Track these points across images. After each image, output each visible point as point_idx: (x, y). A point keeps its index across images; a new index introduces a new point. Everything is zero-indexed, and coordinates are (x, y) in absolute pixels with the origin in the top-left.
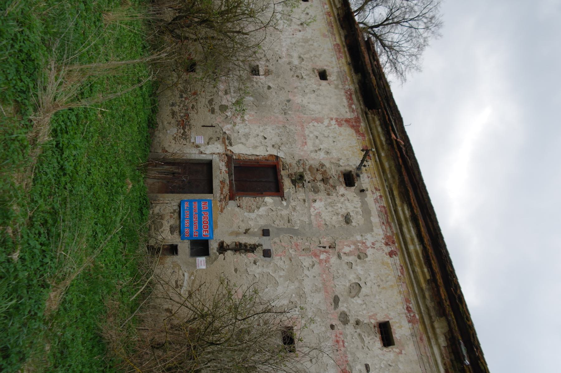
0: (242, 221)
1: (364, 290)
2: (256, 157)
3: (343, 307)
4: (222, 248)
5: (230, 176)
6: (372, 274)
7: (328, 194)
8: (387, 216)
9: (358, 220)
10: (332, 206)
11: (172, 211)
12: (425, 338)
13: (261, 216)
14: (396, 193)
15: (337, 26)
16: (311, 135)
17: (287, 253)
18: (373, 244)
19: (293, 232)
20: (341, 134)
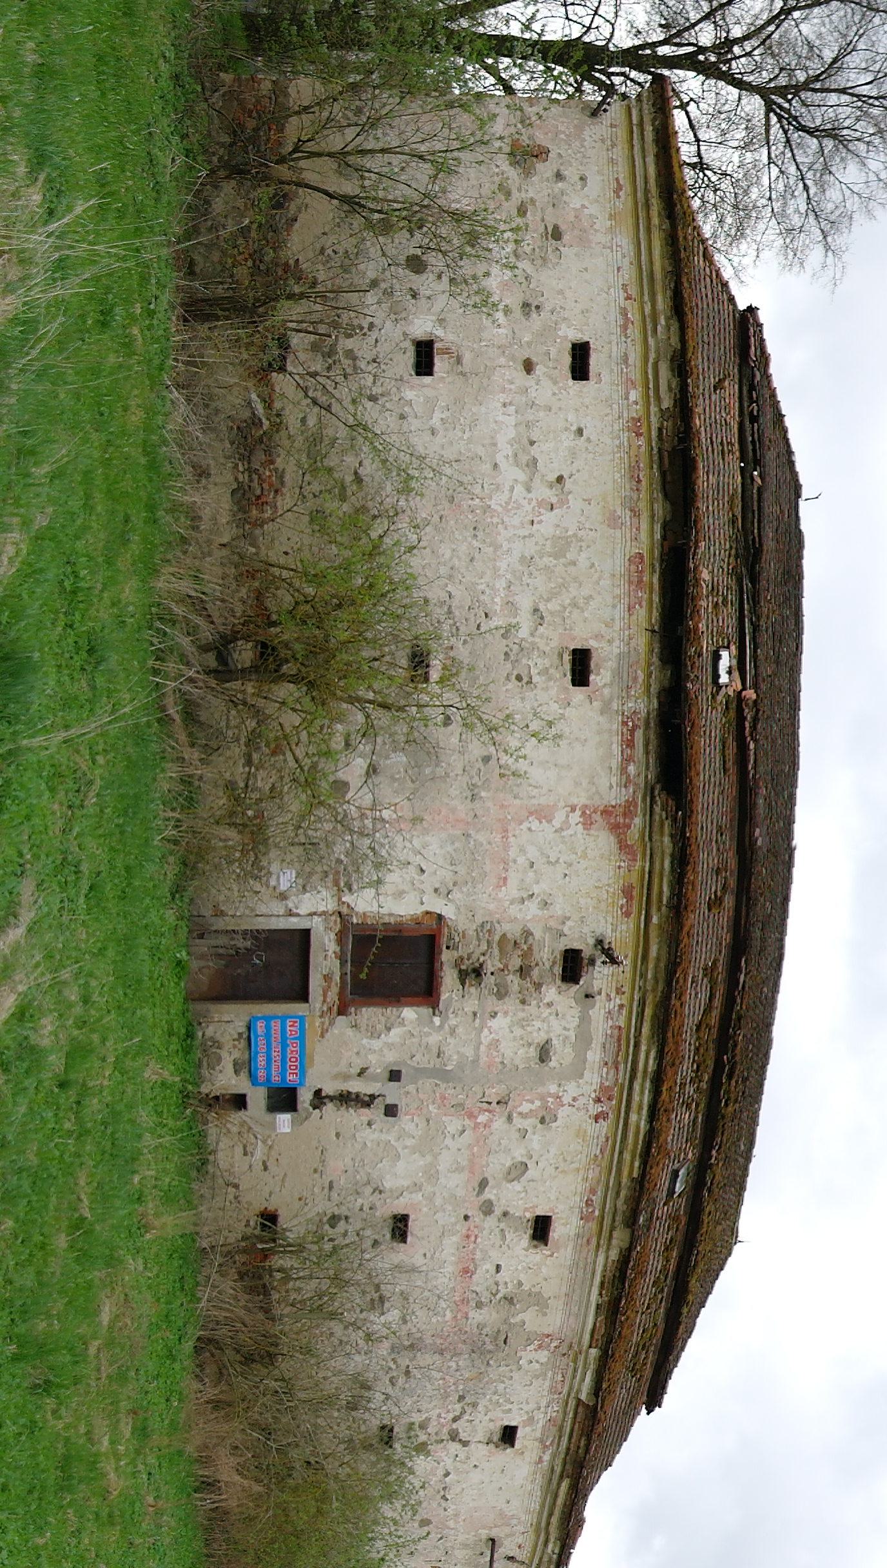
0: (358, 1053)
1: (530, 1174)
2: (399, 919)
3: (489, 1194)
4: (319, 1099)
5: (343, 963)
6: (553, 1151)
7: (523, 1002)
8: (619, 1051)
9: (562, 1055)
10: (523, 1027)
11: (236, 1036)
12: (594, 1241)
13: (390, 1046)
14: (648, 1012)
15: (651, 478)
16: (521, 860)
17: (425, 1111)
18: (574, 1099)
19: (443, 1075)
20: (585, 856)
